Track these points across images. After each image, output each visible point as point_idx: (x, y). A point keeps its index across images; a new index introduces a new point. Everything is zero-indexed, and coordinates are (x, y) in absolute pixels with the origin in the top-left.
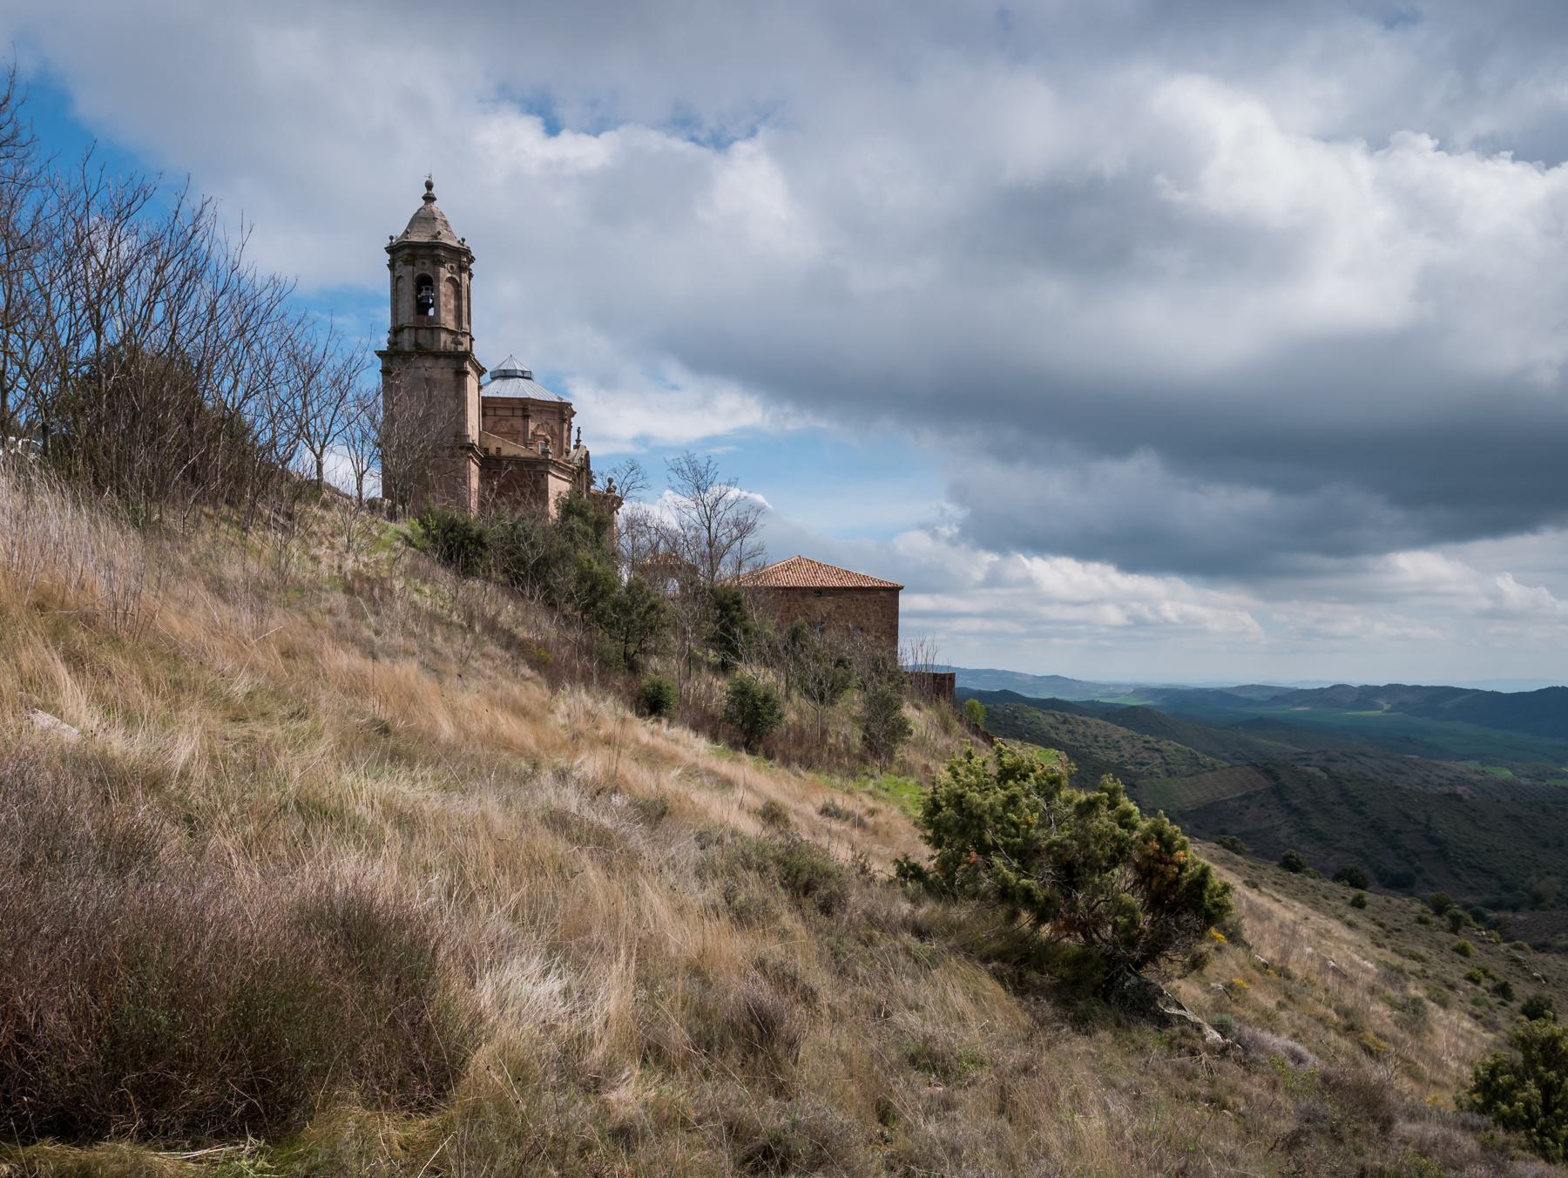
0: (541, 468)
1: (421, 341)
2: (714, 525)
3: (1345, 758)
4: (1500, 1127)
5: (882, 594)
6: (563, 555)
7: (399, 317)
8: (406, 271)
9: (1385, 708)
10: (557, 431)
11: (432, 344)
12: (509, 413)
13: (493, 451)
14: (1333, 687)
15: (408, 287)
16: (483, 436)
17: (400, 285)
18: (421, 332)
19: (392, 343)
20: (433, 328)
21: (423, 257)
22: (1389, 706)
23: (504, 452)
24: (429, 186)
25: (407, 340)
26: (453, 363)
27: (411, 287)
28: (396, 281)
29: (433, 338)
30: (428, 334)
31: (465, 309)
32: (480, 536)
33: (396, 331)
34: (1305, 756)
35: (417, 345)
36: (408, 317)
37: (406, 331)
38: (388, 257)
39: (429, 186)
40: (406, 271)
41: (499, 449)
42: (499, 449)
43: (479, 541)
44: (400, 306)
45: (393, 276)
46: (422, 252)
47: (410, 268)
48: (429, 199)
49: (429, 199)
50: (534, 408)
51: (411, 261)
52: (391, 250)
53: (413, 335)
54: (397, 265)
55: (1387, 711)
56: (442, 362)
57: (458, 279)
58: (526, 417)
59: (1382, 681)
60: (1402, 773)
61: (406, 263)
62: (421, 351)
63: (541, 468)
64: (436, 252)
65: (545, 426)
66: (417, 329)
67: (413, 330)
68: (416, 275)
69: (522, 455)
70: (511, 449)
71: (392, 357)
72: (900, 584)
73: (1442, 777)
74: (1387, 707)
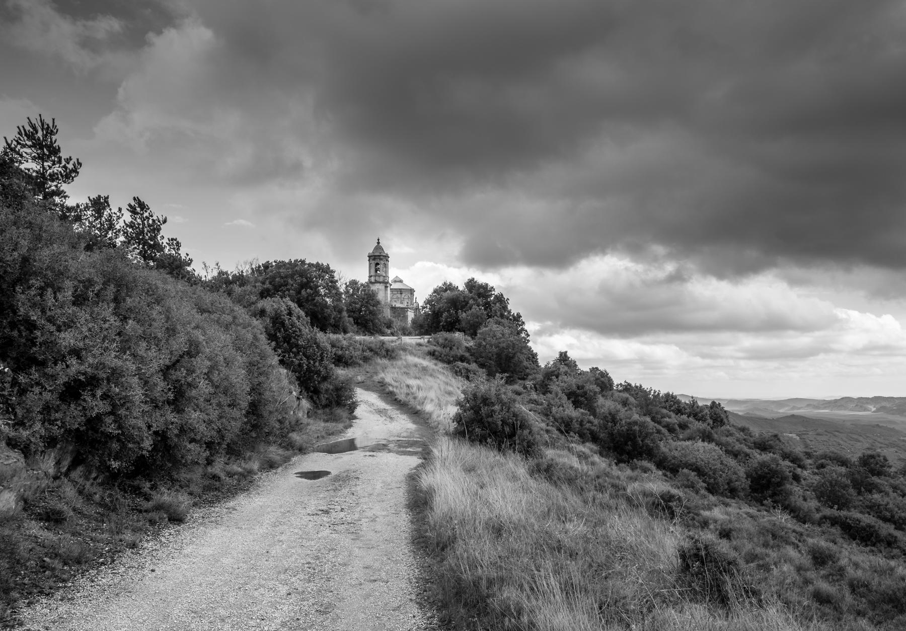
3: (827, 434)
8: (373, 262)
9: (873, 410)
14: (843, 398)
15: (373, 266)
19: (369, 280)
22: (875, 409)
24: (378, 240)
26: (384, 285)
32: (699, 422)
33: (370, 277)
34: (804, 432)
35: (375, 280)
36: (373, 273)
39: (378, 240)
40: (373, 262)
48: (378, 243)
49: (378, 243)
51: (374, 259)
52: (369, 257)
55: (874, 412)
56: (382, 284)
58: (401, 294)
59: (870, 395)
60: (859, 441)
70: (398, 305)
72: (359, 417)
73: (882, 443)
74: (874, 409)
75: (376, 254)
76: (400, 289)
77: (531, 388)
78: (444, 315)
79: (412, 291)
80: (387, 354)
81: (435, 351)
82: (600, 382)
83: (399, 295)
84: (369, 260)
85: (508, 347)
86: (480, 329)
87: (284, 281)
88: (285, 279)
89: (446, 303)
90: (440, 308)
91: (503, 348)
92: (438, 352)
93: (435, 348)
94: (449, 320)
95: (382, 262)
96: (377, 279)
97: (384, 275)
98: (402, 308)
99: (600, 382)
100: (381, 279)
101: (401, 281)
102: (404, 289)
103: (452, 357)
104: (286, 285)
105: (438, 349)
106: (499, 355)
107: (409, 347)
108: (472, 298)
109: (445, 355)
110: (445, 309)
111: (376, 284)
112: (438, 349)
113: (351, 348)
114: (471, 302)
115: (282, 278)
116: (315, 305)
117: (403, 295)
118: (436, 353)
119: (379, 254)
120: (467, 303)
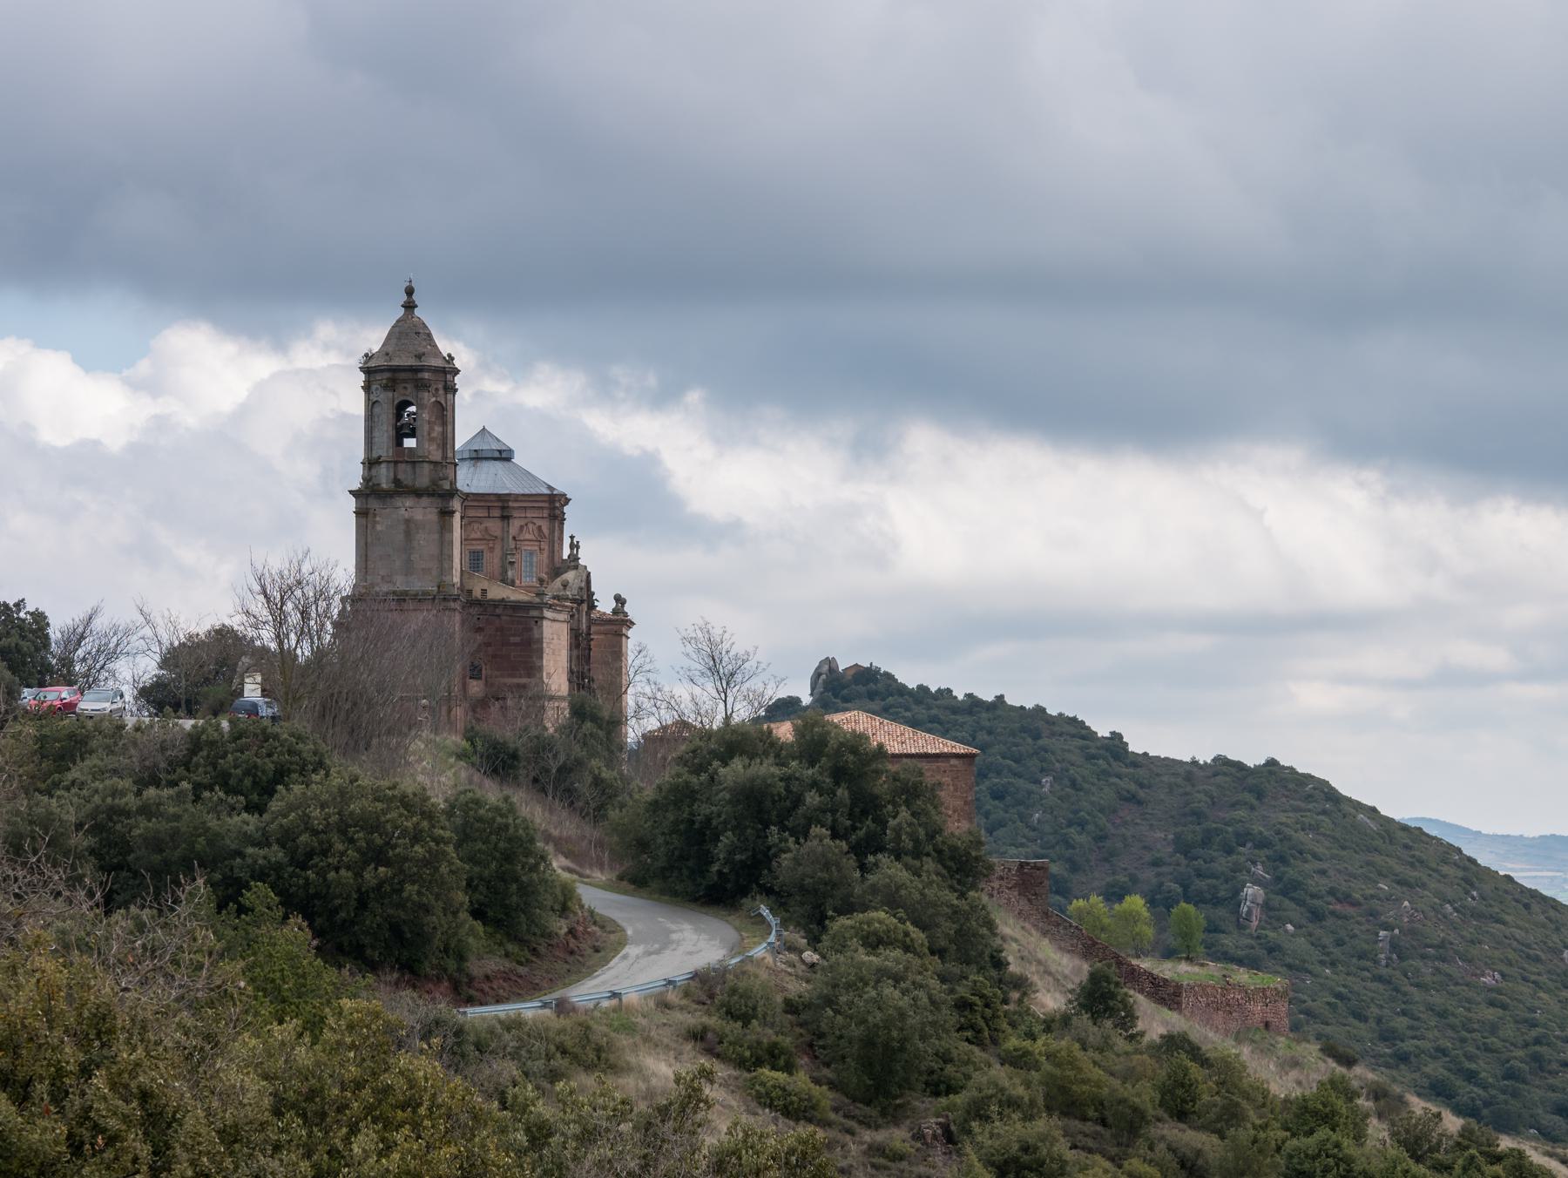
0: (534, 613)
1: (401, 476)
2: (730, 700)
4: (1023, 1087)
5: (953, 761)
6: (579, 763)
7: (375, 448)
10: (545, 530)
11: (414, 479)
12: (482, 513)
13: (477, 593)
16: (466, 576)
17: (377, 410)
18: (401, 467)
20: (414, 462)
21: (405, 381)
23: (490, 595)
24: (410, 292)
25: (384, 476)
26: (438, 502)
27: (391, 416)
28: (371, 405)
29: (415, 473)
30: (409, 468)
31: (449, 435)
33: (370, 463)
35: (397, 481)
36: (384, 449)
37: (383, 465)
38: (362, 376)
39: (410, 292)
41: (484, 591)
42: (484, 591)
43: (514, 756)
44: (376, 434)
45: (368, 400)
46: (403, 375)
47: (390, 394)
49: (410, 306)
50: (516, 505)
52: (368, 371)
53: (392, 470)
54: (374, 387)
56: (425, 501)
57: (443, 402)
58: (505, 518)
61: (386, 388)
62: (400, 489)
63: (534, 613)
64: (420, 375)
65: (530, 526)
66: (396, 463)
67: (392, 465)
68: (396, 402)
69: (512, 598)
71: (369, 498)
75: (396, 362)
76: (499, 497)
77: (935, 1137)
78: (727, 839)
79: (553, 505)
80: (599, 1058)
81: (705, 1029)
82: (1128, 1111)
83: (495, 526)
84: (367, 388)
85: (888, 1025)
86: (841, 841)
87: (321, 843)
88: (323, 836)
89: (730, 802)
90: (708, 819)
91: (876, 1025)
92: (714, 1031)
93: (705, 1019)
94: (738, 857)
95: (428, 398)
96: (405, 474)
97: (436, 455)
98: (517, 607)
99: (1128, 1111)
100: (423, 478)
101: (504, 456)
102: (517, 498)
103: (749, 1048)
104: (325, 853)
105: (713, 1021)
106: (869, 1042)
107: (640, 1020)
108: (814, 784)
109: (730, 1043)
110: (725, 822)
111: (398, 501)
112: (713, 1021)
113: (523, 1053)
114: (812, 799)
115: (315, 833)
116: (401, 905)
117: (515, 525)
118: (710, 1035)
119: (411, 362)
120: (798, 801)
